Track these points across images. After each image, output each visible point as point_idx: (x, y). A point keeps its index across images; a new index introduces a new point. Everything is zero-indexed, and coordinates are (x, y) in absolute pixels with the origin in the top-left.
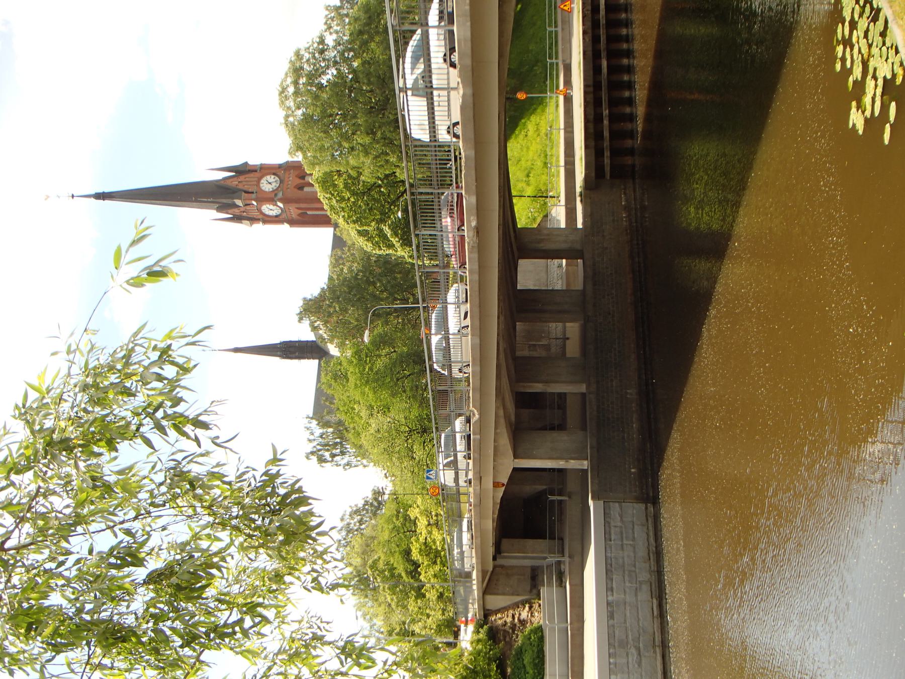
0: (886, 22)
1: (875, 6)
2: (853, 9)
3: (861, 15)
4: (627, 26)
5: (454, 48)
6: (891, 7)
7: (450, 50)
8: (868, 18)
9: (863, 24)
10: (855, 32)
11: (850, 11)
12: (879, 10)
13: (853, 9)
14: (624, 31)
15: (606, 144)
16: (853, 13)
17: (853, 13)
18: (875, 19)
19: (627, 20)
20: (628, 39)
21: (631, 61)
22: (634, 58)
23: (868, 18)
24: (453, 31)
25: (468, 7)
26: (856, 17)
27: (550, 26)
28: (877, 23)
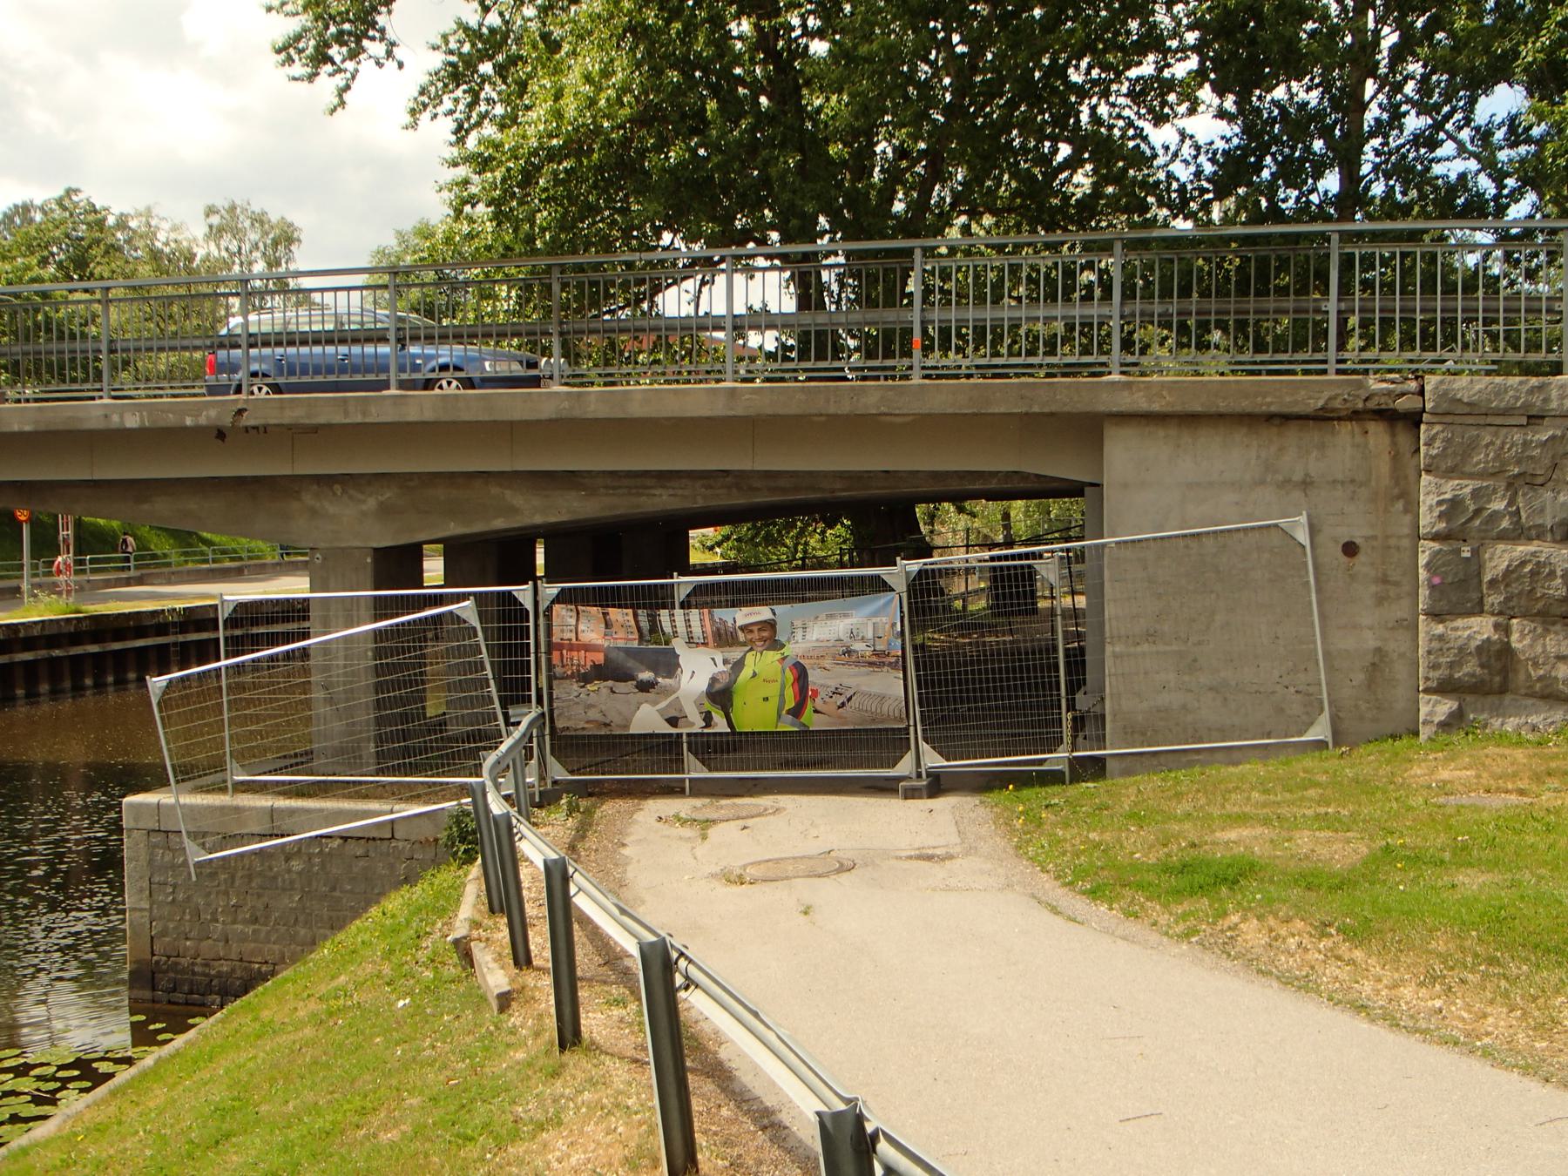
0: (45, 1118)
1: (58, 1096)
2: (48, 1064)
3: (39, 1078)
4: (29, 695)
5: (281, 393)
6: (88, 1107)
7: (470, 379)
8: (38, 1090)
9: (26, 1084)
10: (12, 1076)
11: (44, 1060)
12: (54, 1102)
13: (48, 1064)
14: (44, 688)
15: (42, 654)
16: (42, 1065)
17: (42, 1065)
18: (37, 1100)
19: (105, 685)
20: (55, 693)
21: (111, 689)
22: (74, 698)
23: (38, 1090)
24: (388, 388)
25: (16, 428)
26: (37, 1072)
27: (92, 561)
28: (32, 1105)
